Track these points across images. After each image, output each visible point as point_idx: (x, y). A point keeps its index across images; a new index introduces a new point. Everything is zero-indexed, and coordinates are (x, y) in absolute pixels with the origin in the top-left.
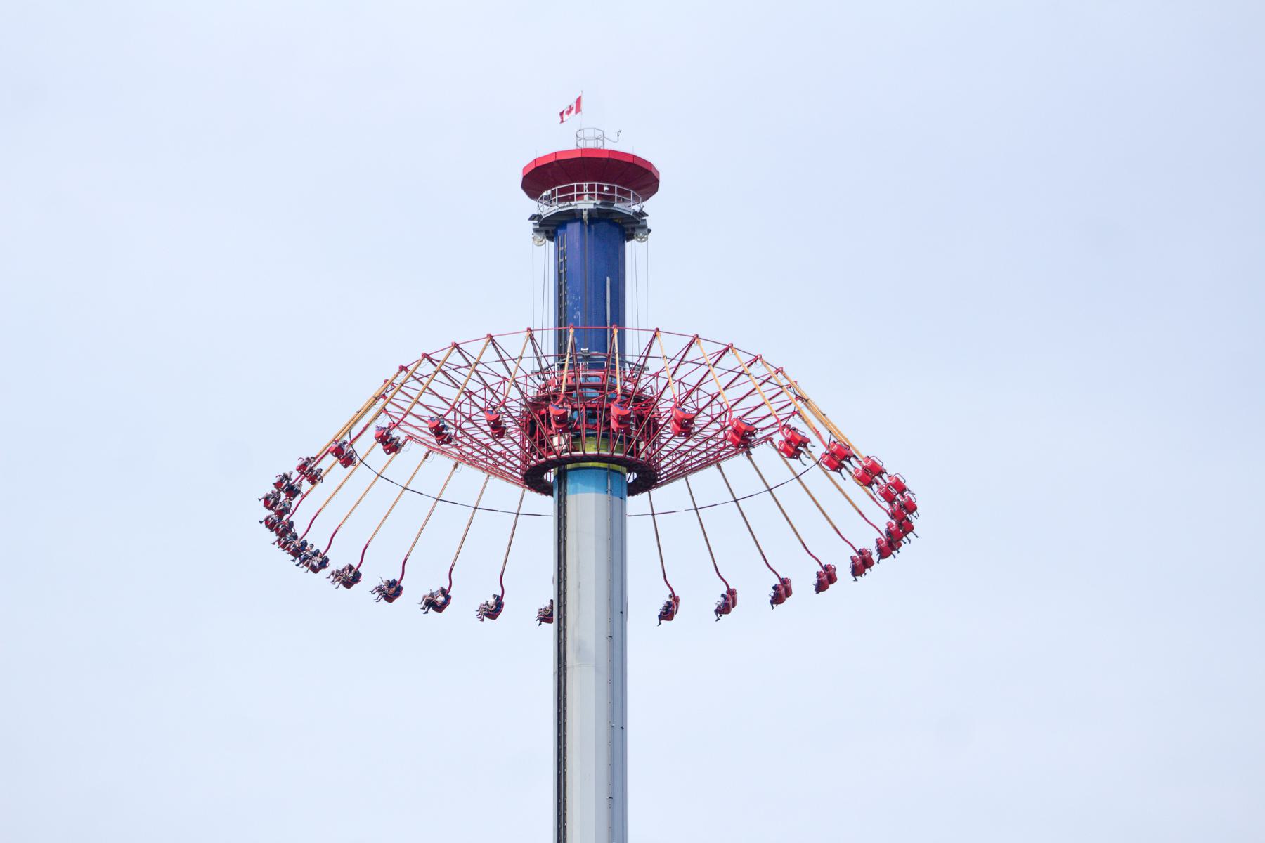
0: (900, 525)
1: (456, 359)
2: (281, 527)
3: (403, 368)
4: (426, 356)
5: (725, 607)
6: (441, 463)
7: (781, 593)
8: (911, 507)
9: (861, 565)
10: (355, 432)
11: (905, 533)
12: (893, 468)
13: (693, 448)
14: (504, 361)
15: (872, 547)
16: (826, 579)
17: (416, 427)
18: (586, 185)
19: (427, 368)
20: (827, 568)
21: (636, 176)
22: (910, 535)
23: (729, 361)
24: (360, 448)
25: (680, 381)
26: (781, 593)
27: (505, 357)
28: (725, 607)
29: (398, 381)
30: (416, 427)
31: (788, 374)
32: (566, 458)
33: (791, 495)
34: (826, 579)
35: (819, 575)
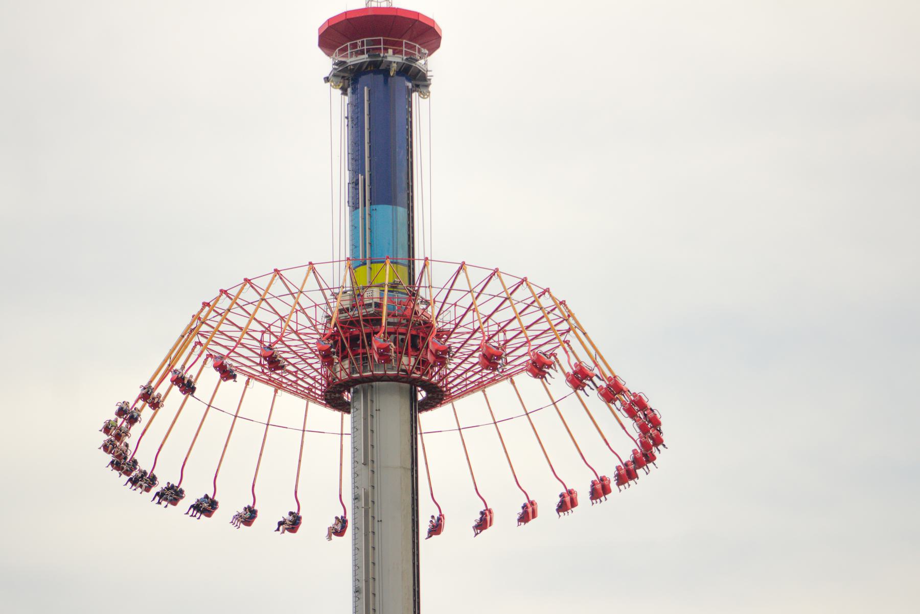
0: (645, 455)
1: (278, 288)
2: (122, 463)
3: (206, 304)
4: (223, 292)
5: (483, 523)
6: (261, 391)
7: (527, 514)
8: (658, 441)
9: (599, 490)
10: (187, 366)
11: (648, 461)
12: (633, 384)
13: (467, 371)
14: (322, 290)
15: (610, 473)
16: (567, 503)
17: (247, 358)
18: (359, 42)
19: (224, 303)
20: (570, 492)
21: (421, 33)
22: (650, 465)
23: (495, 286)
24: (161, 390)
25: (455, 305)
26: (527, 514)
27: (324, 286)
28: (483, 523)
29: (202, 315)
30: (247, 358)
31: (553, 294)
32: (367, 377)
33: (546, 420)
34: (567, 503)
35: (562, 496)
